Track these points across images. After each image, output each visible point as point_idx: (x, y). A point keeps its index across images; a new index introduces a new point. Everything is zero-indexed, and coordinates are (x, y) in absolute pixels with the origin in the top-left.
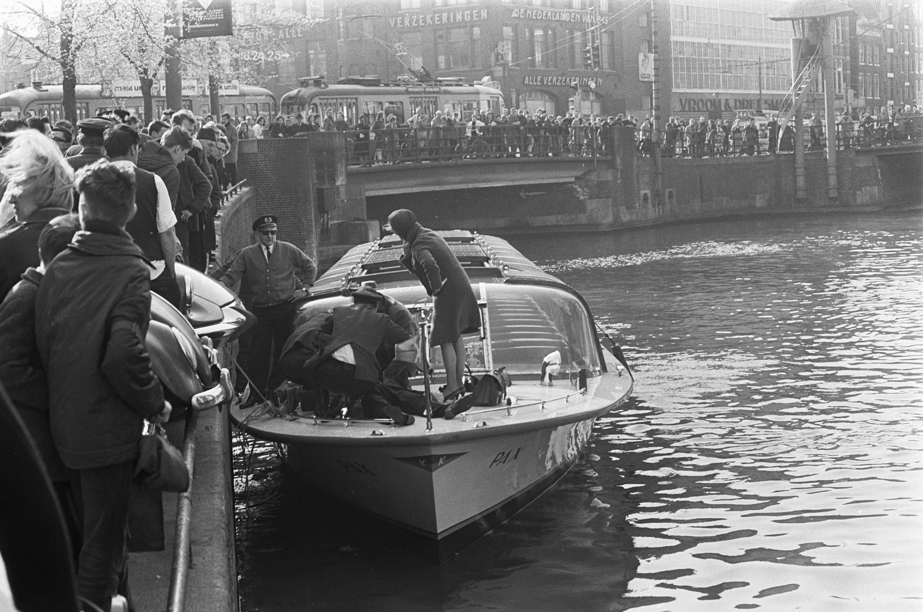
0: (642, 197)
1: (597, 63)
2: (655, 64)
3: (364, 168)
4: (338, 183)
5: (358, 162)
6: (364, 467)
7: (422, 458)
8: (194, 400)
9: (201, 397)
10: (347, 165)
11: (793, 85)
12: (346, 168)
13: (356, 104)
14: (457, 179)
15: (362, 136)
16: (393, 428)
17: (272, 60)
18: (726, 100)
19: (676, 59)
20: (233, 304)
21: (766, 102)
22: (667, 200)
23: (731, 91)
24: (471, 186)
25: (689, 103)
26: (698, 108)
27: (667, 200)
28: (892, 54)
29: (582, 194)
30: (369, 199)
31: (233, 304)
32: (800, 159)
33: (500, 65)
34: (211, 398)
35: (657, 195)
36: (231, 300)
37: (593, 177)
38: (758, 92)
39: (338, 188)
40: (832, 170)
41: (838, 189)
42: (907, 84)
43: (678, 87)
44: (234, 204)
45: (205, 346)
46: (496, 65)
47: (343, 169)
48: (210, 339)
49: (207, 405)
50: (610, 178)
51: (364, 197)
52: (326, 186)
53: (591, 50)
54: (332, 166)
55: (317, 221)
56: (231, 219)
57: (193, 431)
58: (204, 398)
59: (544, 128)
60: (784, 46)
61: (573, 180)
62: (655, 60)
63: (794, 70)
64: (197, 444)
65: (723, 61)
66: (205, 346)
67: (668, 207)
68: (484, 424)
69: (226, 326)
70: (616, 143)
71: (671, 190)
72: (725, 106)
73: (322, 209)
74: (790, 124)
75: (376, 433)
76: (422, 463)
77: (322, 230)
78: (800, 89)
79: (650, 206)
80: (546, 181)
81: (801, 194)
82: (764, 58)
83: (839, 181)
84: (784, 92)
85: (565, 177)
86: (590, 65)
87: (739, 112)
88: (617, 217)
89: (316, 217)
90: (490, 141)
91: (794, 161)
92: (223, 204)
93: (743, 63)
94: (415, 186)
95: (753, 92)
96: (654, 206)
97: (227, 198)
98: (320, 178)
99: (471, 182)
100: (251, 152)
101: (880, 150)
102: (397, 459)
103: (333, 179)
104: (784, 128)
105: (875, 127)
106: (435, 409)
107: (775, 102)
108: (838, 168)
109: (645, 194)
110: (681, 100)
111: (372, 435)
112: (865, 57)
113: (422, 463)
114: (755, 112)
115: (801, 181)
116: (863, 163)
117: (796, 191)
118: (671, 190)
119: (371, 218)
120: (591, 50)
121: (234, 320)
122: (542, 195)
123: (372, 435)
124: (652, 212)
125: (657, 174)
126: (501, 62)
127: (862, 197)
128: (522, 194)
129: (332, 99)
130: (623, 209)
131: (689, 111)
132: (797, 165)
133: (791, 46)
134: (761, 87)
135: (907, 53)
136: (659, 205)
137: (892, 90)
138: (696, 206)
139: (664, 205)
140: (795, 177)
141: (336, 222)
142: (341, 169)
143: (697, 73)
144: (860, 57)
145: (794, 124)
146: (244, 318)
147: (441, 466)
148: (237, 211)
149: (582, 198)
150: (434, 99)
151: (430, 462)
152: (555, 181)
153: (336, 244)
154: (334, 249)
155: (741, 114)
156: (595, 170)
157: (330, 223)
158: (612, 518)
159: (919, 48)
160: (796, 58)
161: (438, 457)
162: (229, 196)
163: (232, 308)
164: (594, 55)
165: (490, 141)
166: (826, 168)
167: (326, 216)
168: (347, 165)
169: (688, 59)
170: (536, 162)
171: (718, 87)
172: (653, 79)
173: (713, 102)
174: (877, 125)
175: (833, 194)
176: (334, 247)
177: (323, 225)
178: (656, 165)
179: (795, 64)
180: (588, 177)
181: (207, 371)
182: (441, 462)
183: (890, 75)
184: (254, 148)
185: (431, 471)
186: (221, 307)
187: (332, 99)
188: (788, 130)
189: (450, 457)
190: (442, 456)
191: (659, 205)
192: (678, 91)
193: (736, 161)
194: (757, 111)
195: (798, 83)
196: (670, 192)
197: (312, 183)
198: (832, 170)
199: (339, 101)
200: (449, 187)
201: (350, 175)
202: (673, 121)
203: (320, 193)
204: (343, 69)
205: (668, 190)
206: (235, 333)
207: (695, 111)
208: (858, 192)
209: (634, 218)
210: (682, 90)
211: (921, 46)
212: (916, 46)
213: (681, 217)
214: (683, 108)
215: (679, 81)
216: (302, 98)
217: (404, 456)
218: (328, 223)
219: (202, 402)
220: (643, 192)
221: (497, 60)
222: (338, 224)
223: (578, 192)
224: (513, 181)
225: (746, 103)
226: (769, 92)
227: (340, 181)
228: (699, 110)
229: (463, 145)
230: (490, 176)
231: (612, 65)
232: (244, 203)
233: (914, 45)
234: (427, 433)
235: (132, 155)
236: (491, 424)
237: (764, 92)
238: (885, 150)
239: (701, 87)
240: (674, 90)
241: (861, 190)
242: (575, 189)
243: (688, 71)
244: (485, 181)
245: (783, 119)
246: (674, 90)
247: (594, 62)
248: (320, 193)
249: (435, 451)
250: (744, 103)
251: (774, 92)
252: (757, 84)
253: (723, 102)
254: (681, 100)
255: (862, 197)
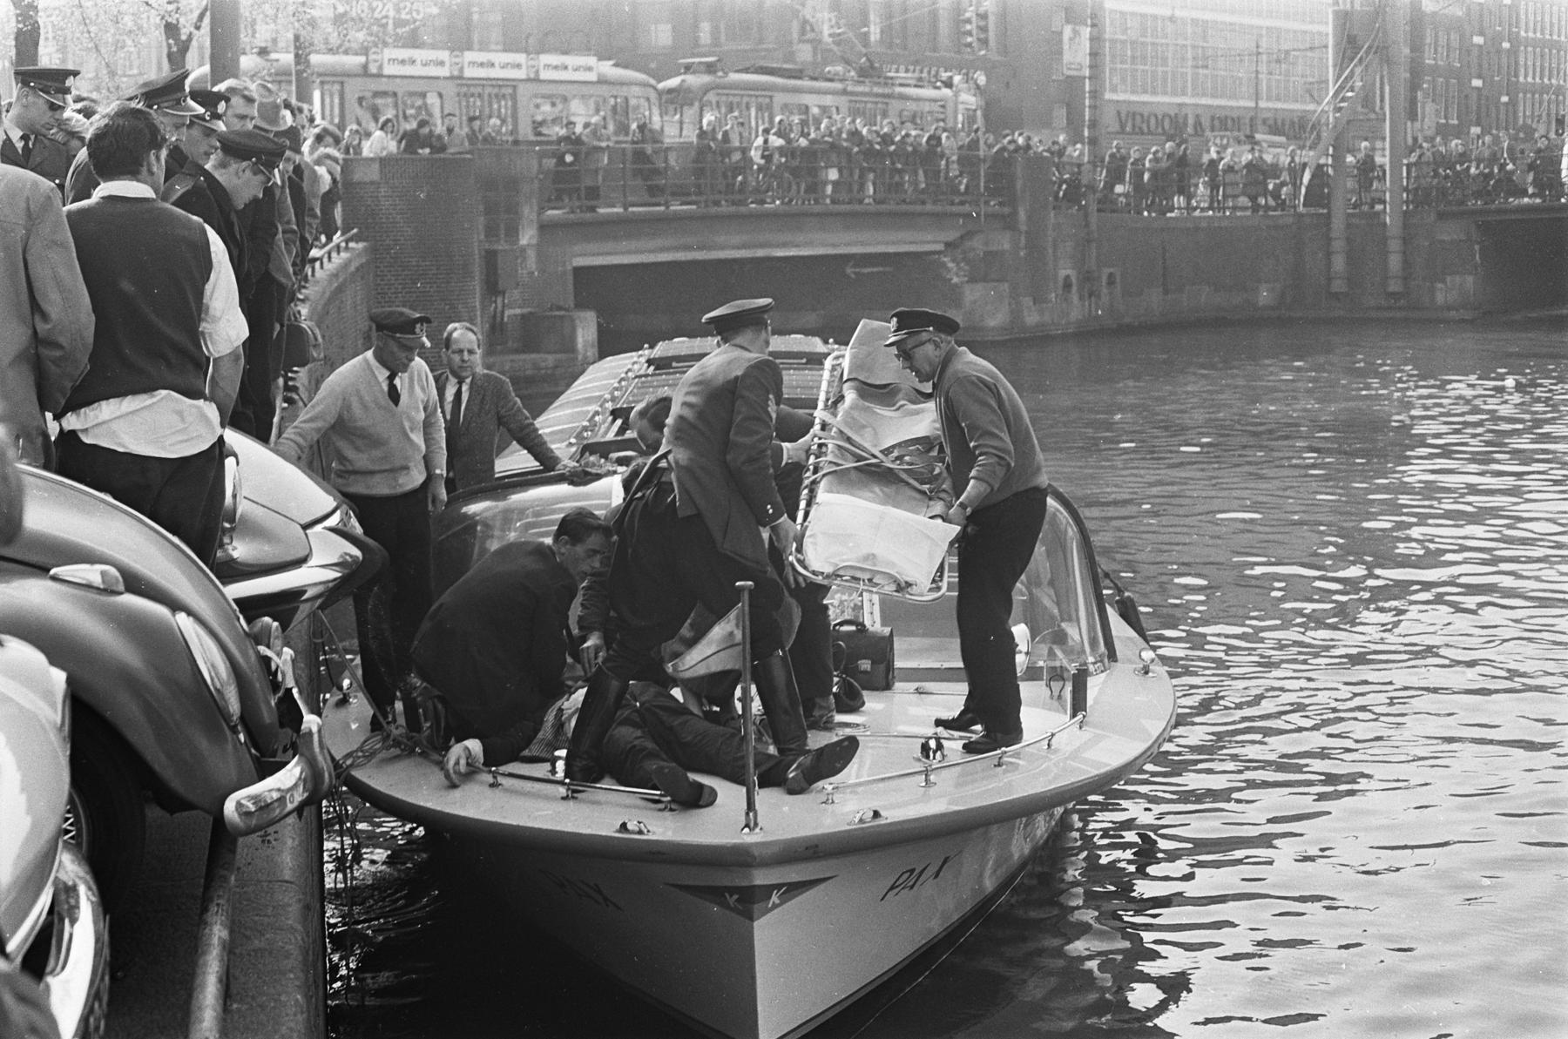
0: (1061, 283)
1: (984, 42)
2: (1091, 48)
3: (572, 216)
4: (524, 241)
5: (560, 204)
6: (600, 892)
7: (732, 890)
8: (230, 807)
9: (251, 798)
10: (542, 209)
11: (1331, 94)
12: (539, 214)
13: (770, 107)
14: (736, 239)
15: (569, 158)
16: (667, 814)
17: (408, 17)
18: (1197, 116)
19: (1113, 41)
20: (333, 521)
21: (1264, 121)
22: (1105, 291)
23: (1204, 101)
24: (760, 253)
25: (1134, 119)
26: (1148, 127)
27: (1105, 291)
28: (1480, 46)
29: (955, 273)
30: (578, 271)
31: (333, 521)
32: (1338, 224)
33: (808, 41)
34: (275, 795)
35: (1087, 278)
36: (330, 509)
37: (977, 244)
38: (1252, 104)
39: (523, 250)
40: (1394, 245)
41: (1405, 279)
42: (1505, 99)
43: (1114, 90)
44: (335, 275)
45: (262, 649)
46: (800, 41)
47: (534, 216)
48: (276, 624)
49: (265, 816)
50: (1007, 246)
51: (569, 268)
52: (501, 246)
53: (974, 19)
54: (513, 210)
55: (483, 309)
56: (330, 301)
57: (226, 879)
58: (255, 799)
59: (891, 154)
60: (1322, 28)
61: (940, 247)
62: (1091, 39)
63: (1335, 66)
64: (234, 928)
65: (1194, 47)
66: (262, 649)
67: (1105, 299)
68: (876, 814)
69: (313, 575)
70: (1019, 184)
71: (1112, 270)
72: (1195, 128)
73: (493, 288)
74: (1322, 161)
75: (630, 827)
76: (732, 900)
77: (493, 328)
78: (1343, 100)
79: (1075, 298)
80: (891, 249)
81: (1338, 286)
82: (1264, 44)
83: (1407, 264)
84: (1311, 107)
85: (926, 241)
86: (970, 45)
87: (1215, 137)
88: (1016, 314)
89: (482, 303)
90: (795, 172)
91: (1328, 225)
92: (313, 275)
93: (1220, 53)
94: (663, 250)
95: (1242, 103)
96: (1081, 298)
97: (322, 264)
98: (491, 231)
99: (762, 246)
100: (367, 179)
101: (1481, 212)
102: (673, 885)
103: (513, 232)
104: (1314, 166)
105: (1473, 170)
106: (764, 768)
107: (1279, 123)
108: (1406, 240)
109: (1068, 277)
110: (1119, 113)
111: (619, 831)
112: (1436, 50)
113: (732, 900)
114: (1243, 138)
115: (1339, 263)
116: (1450, 233)
117: (1329, 279)
118: (1112, 270)
119: (581, 305)
120: (974, 19)
121: (335, 560)
122: (884, 273)
123: (619, 831)
124: (1077, 310)
125: (1089, 241)
126: (810, 36)
127: (1443, 294)
128: (849, 270)
129: (735, 95)
130: (1027, 301)
131: (1133, 133)
132: (1333, 235)
133: (1330, 29)
134: (1257, 97)
135: (1506, 45)
136: (1090, 296)
137: (1479, 108)
138: (1154, 301)
139: (1099, 297)
140: (1329, 254)
141: (518, 311)
142: (528, 212)
143: (1160, 69)
144: (1427, 47)
145: (1330, 161)
146: (356, 552)
147: (775, 906)
148: (340, 290)
149: (955, 280)
150: (767, 100)
151: (749, 901)
152: (913, 248)
153: (517, 351)
154: (512, 361)
155: (1218, 141)
156: (981, 231)
157: (507, 313)
158: (1107, 1000)
159: (1527, 38)
160: (1337, 45)
161: (768, 890)
162: (325, 260)
163: (332, 530)
164: (979, 28)
165: (795, 172)
166: (1384, 240)
167: (499, 300)
168: (542, 209)
169: (1133, 43)
170: (879, 214)
171: (1184, 93)
172: (1087, 73)
173: (1174, 119)
174: (1477, 168)
175: (1394, 286)
176: (512, 357)
177: (494, 317)
178: (1087, 225)
179: (1336, 53)
180: (968, 244)
181: (266, 715)
182: (775, 899)
183: (1477, 83)
184: (373, 174)
185: (752, 919)
186: (306, 527)
187: (735, 95)
188: (1319, 171)
189: (794, 889)
190: (778, 886)
191: (1090, 296)
192: (1115, 97)
193: (1225, 223)
194: (1247, 137)
195: (1341, 88)
196: (1111, 275)
197: (477, 241)
198: (1394, 245)
199: (745, 99)
200: (722, 255)
201: (545, 228)
202: (1118, 148)
203: (490, 258)
204: (531, 40)
205: (1106, 271)
206: (332, 593)
207: (1143, 133)
208: (1440, 285)
209: (1047, 318)
210: (1121, 97)
211: (1563, 38)
212: (1523, 33)
213: (1127, 320)
214: (1123, 126)
215: (1116, 80)
216: (689, 90)
217: (691, 883)
218: (503, 312)
219: (253, 808)
220: (1063, 273)
221: (803, 32)
222: (523, 316)
223: (949, 270)
224: (834, 246)
225: (1229, 122)
226: (1271, 105)
227: (528, 237)
228: (1150, 133)
229: (750, 178)
230: (788, 237)
231: (1004, 50)
232: (353, 274)
233: (1518, 33)
234: (749, 838)
235: (151, 173)
236: (892, 815)
237: (1262, 104)
238: (1489, 212)
239: (1154, 93)
240: (1108, 96)
241: (1444, 281)
242: (944, 265)
243: (1133, 63)
244: (784, 245)
245: (1312, 153)
246: (1108, 96)
247: (979, 39)
248: (490, 258)
249: (761, 878)
250: (1225, 122)
251: (1279, 105)
252: (1252, 91)
253: (1191, 121)
254: (1119, 113)
255: (1443, 294)
